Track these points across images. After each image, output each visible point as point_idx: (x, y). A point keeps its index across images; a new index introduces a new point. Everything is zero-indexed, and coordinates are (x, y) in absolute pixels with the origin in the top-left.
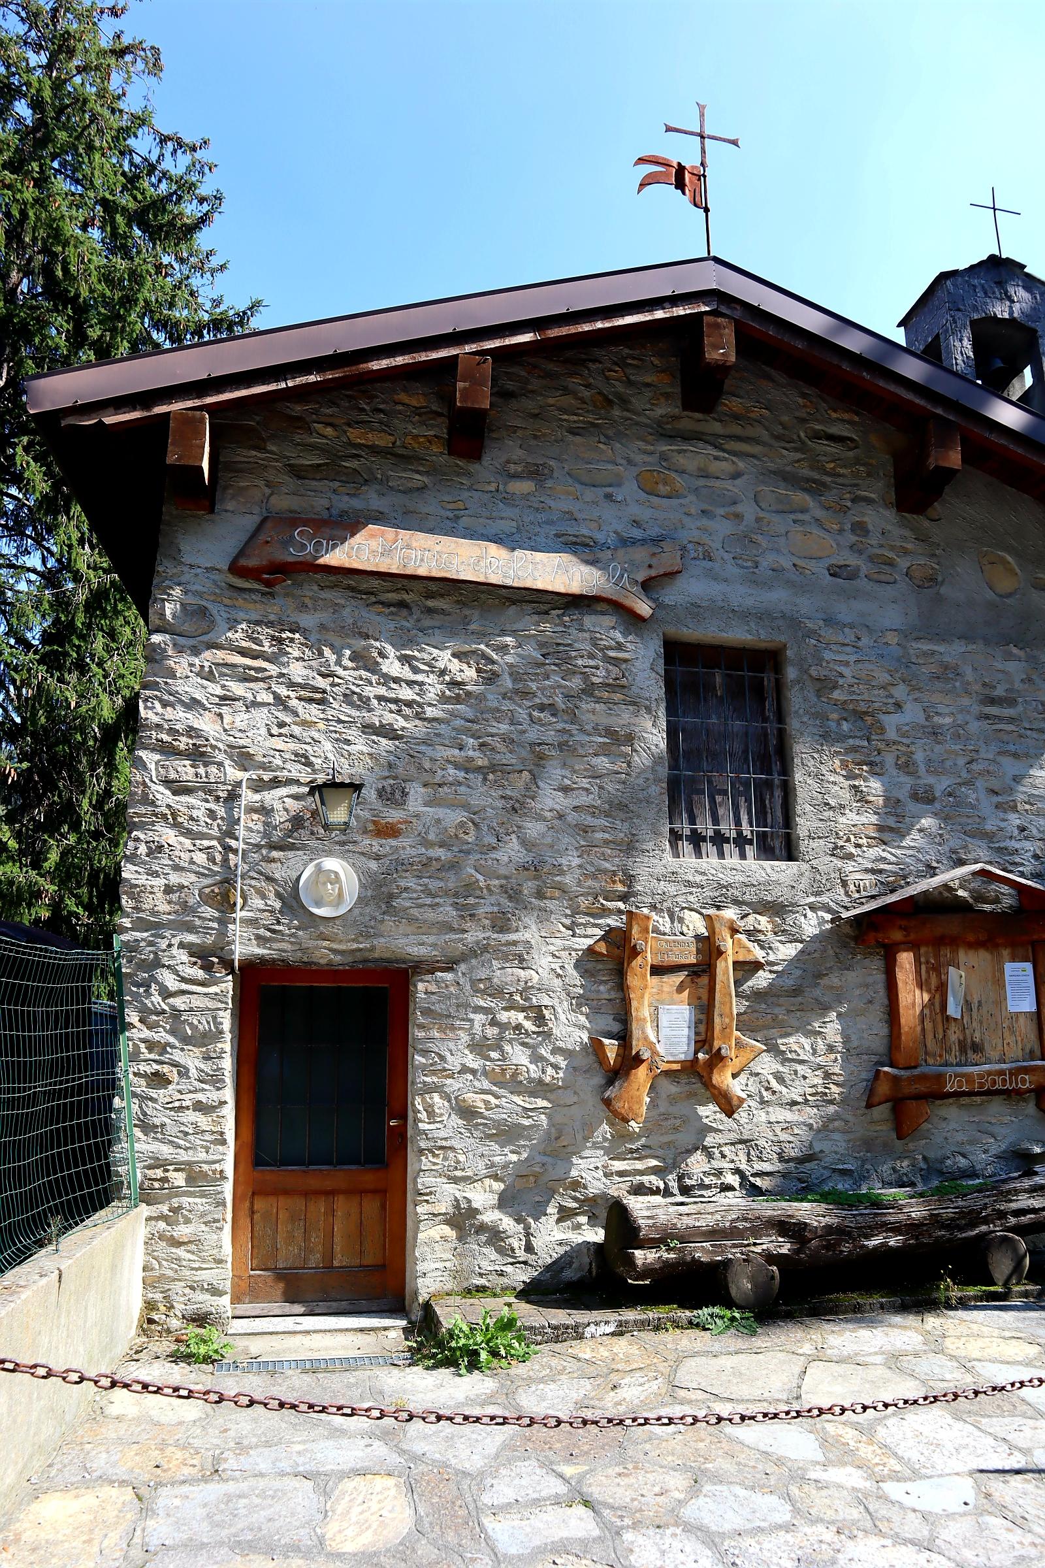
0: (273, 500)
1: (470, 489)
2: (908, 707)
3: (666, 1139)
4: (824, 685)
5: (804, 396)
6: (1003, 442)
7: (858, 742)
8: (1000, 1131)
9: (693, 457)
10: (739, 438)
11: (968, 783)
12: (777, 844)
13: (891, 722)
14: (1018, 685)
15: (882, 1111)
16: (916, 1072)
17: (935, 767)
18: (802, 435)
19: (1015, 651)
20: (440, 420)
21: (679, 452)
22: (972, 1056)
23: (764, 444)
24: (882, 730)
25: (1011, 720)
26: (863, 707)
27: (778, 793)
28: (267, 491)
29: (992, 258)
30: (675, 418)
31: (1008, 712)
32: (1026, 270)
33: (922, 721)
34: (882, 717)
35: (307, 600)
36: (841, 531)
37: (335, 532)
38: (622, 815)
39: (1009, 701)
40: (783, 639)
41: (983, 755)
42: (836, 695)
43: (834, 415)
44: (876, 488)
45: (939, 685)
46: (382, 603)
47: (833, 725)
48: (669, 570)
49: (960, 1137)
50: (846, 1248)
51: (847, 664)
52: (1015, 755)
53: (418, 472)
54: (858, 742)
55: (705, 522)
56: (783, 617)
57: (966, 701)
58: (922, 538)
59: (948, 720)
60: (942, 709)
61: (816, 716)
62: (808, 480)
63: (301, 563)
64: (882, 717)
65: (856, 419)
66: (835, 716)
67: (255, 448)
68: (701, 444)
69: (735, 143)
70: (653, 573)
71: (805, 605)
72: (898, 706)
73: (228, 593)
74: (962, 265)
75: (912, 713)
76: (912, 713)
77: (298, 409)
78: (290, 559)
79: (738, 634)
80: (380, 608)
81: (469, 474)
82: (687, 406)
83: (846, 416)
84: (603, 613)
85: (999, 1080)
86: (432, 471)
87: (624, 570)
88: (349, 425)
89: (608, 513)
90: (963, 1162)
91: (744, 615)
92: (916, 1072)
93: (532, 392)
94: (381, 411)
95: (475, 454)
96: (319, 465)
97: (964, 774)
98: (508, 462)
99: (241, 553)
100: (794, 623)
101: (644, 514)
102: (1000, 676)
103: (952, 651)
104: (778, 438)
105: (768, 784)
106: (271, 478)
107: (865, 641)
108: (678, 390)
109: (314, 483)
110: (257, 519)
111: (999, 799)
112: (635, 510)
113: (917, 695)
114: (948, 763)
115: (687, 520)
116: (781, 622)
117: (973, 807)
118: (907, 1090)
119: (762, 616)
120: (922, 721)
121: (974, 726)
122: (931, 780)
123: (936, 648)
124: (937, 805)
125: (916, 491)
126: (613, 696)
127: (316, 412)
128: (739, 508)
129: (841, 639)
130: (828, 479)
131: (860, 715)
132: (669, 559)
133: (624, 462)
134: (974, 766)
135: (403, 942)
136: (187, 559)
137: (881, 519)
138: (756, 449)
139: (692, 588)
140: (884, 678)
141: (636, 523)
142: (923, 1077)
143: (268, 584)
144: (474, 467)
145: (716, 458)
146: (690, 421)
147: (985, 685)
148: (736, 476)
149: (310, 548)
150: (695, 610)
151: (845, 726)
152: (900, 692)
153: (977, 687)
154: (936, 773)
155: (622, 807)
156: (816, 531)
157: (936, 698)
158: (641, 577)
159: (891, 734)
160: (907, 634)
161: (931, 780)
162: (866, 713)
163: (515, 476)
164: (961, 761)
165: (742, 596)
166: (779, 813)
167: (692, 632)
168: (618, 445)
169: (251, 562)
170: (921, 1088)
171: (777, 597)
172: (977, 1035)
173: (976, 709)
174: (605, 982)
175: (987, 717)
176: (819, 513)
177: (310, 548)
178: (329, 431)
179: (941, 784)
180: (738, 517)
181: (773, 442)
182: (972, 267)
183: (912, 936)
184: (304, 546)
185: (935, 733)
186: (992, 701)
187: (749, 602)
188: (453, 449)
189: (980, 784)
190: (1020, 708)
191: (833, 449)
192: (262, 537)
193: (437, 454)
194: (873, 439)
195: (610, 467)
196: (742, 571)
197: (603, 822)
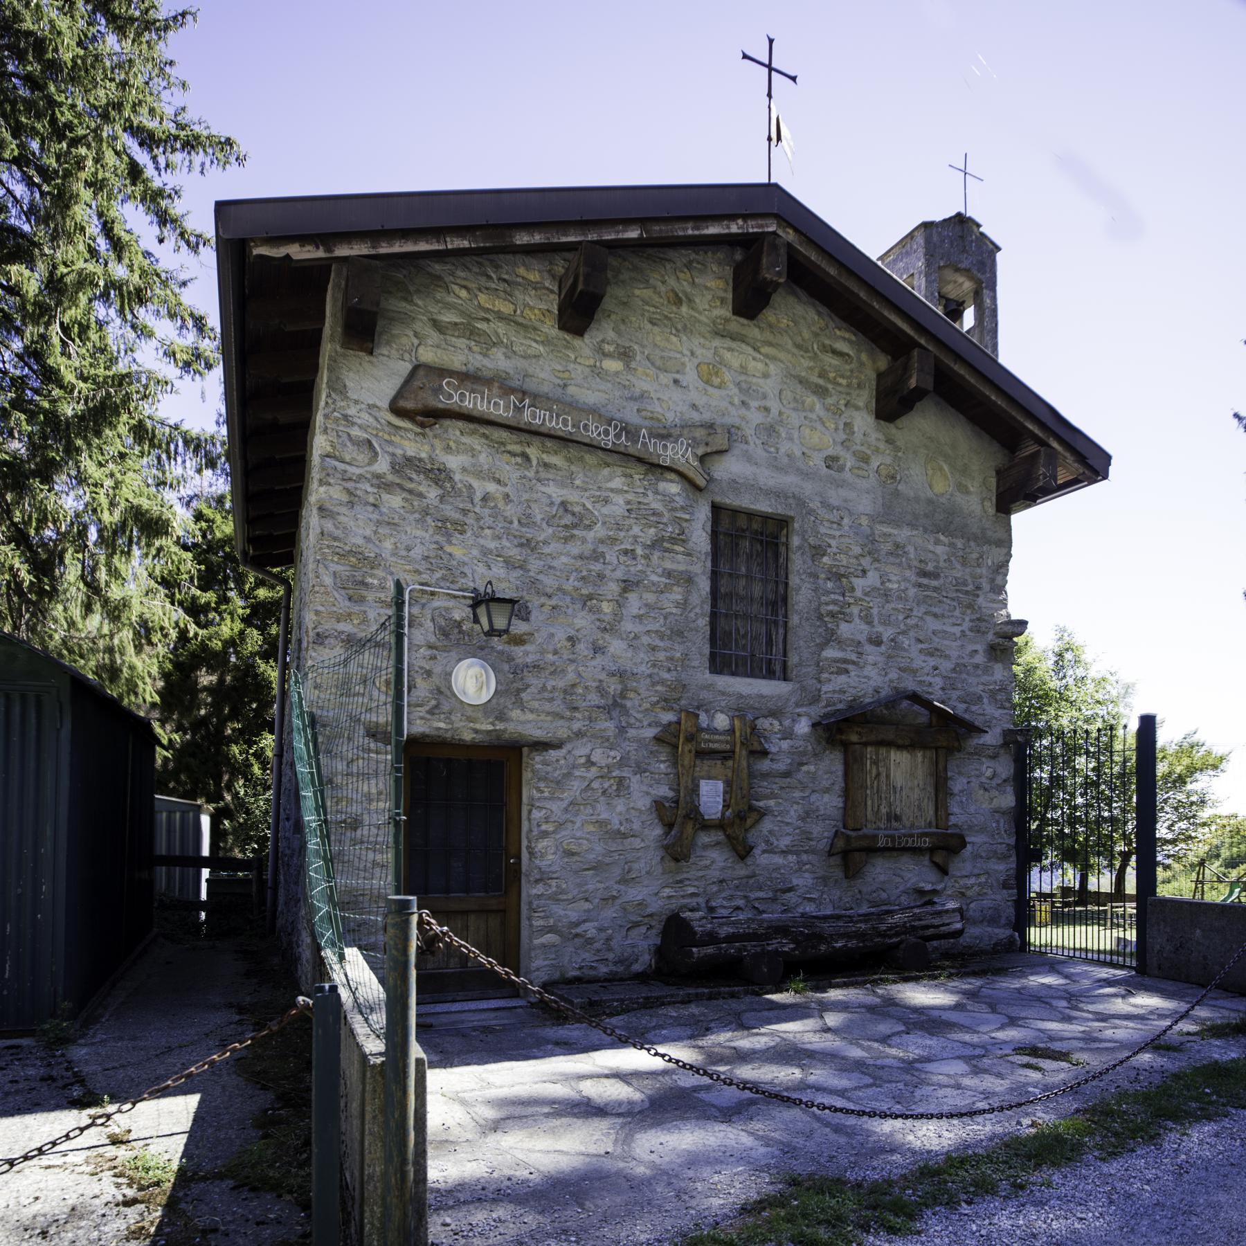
0: (421, 350)
1: (575, 361)
2: (870, 574)
3: (701, 873)
4: (818, 551)
5: (819, 314)
6: (962, 372)
7: (837, 597)
8: (1128, 933)
9: (735, 356)
10: (771, 344)
11: (904, 633)
12: (778, 668)
13: (859, 583)
14: (942, 564)
15: (836, 860)
16: (860, 833)
17: (886, 622)
18: (815, 347)
19: (942, 537)
20: (552, 296)
21: (729, 349)
22: (895, 824)
23: (788, 352)
24: (853, 589)
25: (935, 589)
26: (842, 571)
27: (781, 631)
28: (416, 342)
29: (959, 215)
30: (727, 320)
31: (934, 583)
32: (981, 229)
33: (878, 585)
34: (854, 580)
35: (451, 444)
36: (836, 429)
37: (475, 387)
38: (679, 640)
39: (934, 575)
40: (791, 513)
41: (915, 613)
42: (825, 559)
43: (838, 333)
44: (865, 397)
45: (892, 559)
46: (509, 452)
47: (821, 582)
48: (720, 448)
49: (882, 878)
50: (823, 948)
51: (834, 537)
52: (935, 616)
53: (536, 341)
54: (837, 597)
55: (743, 411)
56: (794, 496)
57: (908, 573)
58: (890, 441)
59: (896, 586)
60: (894, 578)
61: (811, 575)
62: (817, 385)
63: (449, 410)
64: (854, 580)
65: (853, 338)
66: (823, 576)
67: (405, 299)
68: (743, 346)
69: (794, 79)
70: (709, 450)
71: (808, 488)
72: (864, 572)
73: (387, 429)
74: (938, 218)
75: (872, 579)
76: (872, 579)
77: (437, 268)
78: (440, 406)
79: (764, 506)
80: (506, 457)
81: (574, 349)
82: (737, 311)
83: (847, 335)
84: (672, 481)
85: (910, 841)
86: (546, 342)
87: (689, 445)
88: (480, 290)
89: (676, 394)
90: (884, 895)
91: (767, 492)
92: (860, 833)
93: (623, 282)
94: (505, 280)
95: (579, 332)
96: (456, 324)
97: (902, 626)
98: (603, 341)
99: (399, 395)
100: (801, 503)
101: (701, 401)
102: (930, 555)
103: (902, 534)
104: (799, 347)
105: (776, 623)
106: (418, 330)
107: (846, 521)
108: (730, 296)
109: (454, 339)
110: (409, 367)
111: (923, 646)
112: (694, 396)
113: (877, 565)
114: (893, 617)
115: (731, 408)
116: (791, 501)
117: (905, 650)
118: (855, 845)
119: (778, 494)
120: (878, 585)
121: (912, 592)
122: (880, 629)
123: (893, 531)
124: (883, 648)
125: (892, 405)
126: (676, 547)
127: (453, 274)
128: (768, 404)
129: (831, 517)
130: (830, 386)
131: (839, 577)
132: (720, 441)
133: (688, 353)
134: (908, 621)
135: (524, 723)
136: (352, 395)
137: (863, 422)
138: (782, 355)
139: (729, 468)
140: (857, 550)
141: (694, 406)
142: (865, 836)
143: (422, 425)
144: (577, 342)
145: (754, 359)
146: (738, 324)
147: (921, 561)
148: (766, 376)
149: (456, 398)
150: (734, 485)
151: (830, 585)
152: (866, 562)
153: (916, 563)
154: (884, 624)
155: (680, 633)
156: (819, 426)
157: (889, 569)
158: (700, 452)
159: (858, 593)
160: (873, 519)
161: (880, 629)
162: (843, 576)
163: (606, 355)
164: (901, 617)
165: (768, 478)
166: (781, 646)
167: (731, 500)
168: (684, 338)
169: (409, 404)
170: (864, 843)
171: (789, 481)
172: (898, 809)
173: (914, 578)
174: (664, 762)
175: (920, 585)
176: (822, 413)
177: (456, 398)
178: (464, 293)
179: (887, 633)
180: (767, 410)
181: (795, 351)
182: (945, 220)
183: (864, 739)
184: (450, 396)
185: (886, 595)
186: (924, 574)
187: (771, 483)
188: (563, 327)
189: (912, 634)
190: (941, 581)
191: (835, 361)
192: (417, 384)
193: (550, 328)
194: (864, 357)
195: (679, 356)
196: (765, 454)
197: (668, 644)
